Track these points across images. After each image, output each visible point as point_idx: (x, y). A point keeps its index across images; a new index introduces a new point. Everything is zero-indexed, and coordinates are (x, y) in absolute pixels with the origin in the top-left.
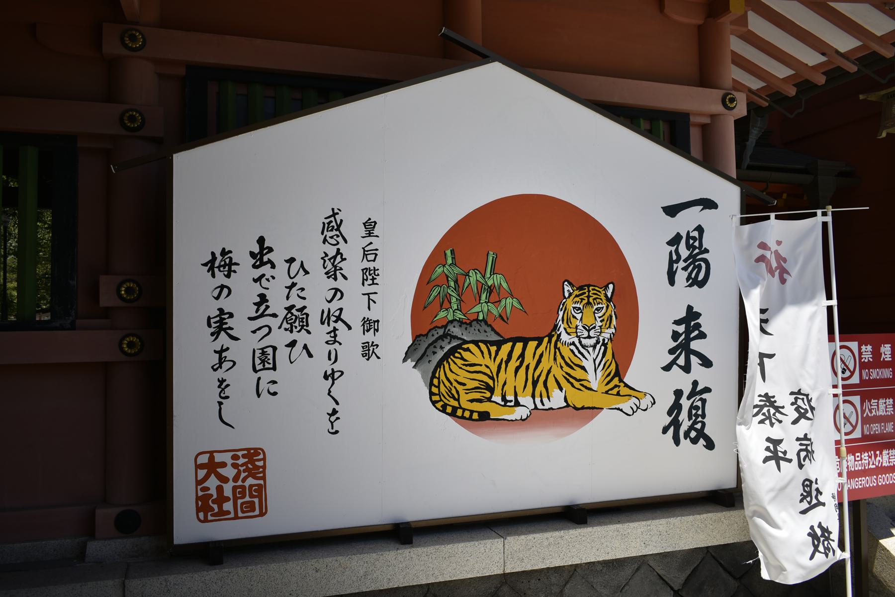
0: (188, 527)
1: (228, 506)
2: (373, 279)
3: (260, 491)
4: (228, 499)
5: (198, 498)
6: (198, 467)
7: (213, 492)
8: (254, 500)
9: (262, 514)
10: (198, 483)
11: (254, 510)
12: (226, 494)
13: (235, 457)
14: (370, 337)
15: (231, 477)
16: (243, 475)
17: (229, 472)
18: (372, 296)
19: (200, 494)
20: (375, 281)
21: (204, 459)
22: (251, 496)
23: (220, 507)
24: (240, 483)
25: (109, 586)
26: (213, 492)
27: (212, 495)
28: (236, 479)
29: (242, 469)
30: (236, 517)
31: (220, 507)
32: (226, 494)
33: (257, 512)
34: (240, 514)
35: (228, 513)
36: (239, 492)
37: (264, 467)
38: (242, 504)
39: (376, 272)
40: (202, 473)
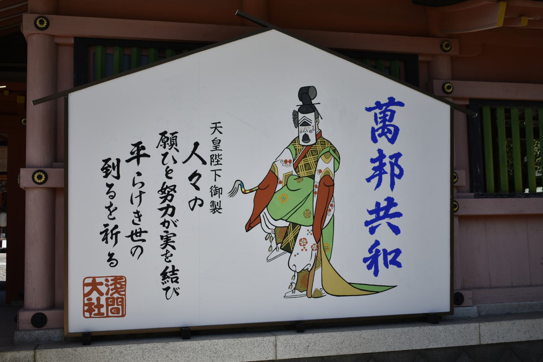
0: (78, 321)
1: (103, 310)
2: (218, 161)
3: (123, 302)
4: (103, 306)
5: (85, 305)
6: (85, 285)
7: (94, 301)
8: (118, 306)
9: (123, 316)
10: (85, 295)
11: (119, 313)
12: (101, 303)
13: (107, 280)
14: (216, 198)
15: (104, 292)
16: (111, 292)
17: (103, 289)
18: (218, 172)
19: (86, 302)
20: (219, 163)
21: (90, 281)
22: (118, 305)
23: (99, 311)
24: (109, 296)
25: (26, 354)
26: (94, 301)
27: (94, 304)
28: (107, 293)
29: (111, 287)
30: (108, 316)
31: (99, 311)
32: (101, 303)
33: (120, 314)
34: (110, 314)
35: (103, 314)
36: (110, 301)
37: (125, 285)
38: (111, 309)
39: (220, 157)
40: (87, 289)
